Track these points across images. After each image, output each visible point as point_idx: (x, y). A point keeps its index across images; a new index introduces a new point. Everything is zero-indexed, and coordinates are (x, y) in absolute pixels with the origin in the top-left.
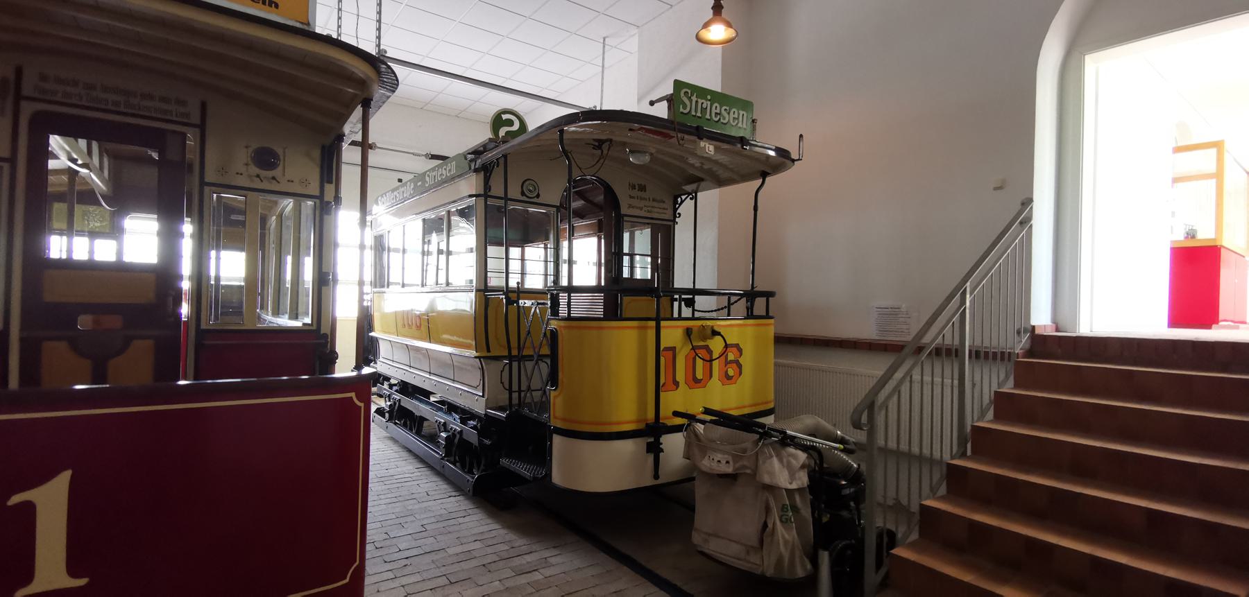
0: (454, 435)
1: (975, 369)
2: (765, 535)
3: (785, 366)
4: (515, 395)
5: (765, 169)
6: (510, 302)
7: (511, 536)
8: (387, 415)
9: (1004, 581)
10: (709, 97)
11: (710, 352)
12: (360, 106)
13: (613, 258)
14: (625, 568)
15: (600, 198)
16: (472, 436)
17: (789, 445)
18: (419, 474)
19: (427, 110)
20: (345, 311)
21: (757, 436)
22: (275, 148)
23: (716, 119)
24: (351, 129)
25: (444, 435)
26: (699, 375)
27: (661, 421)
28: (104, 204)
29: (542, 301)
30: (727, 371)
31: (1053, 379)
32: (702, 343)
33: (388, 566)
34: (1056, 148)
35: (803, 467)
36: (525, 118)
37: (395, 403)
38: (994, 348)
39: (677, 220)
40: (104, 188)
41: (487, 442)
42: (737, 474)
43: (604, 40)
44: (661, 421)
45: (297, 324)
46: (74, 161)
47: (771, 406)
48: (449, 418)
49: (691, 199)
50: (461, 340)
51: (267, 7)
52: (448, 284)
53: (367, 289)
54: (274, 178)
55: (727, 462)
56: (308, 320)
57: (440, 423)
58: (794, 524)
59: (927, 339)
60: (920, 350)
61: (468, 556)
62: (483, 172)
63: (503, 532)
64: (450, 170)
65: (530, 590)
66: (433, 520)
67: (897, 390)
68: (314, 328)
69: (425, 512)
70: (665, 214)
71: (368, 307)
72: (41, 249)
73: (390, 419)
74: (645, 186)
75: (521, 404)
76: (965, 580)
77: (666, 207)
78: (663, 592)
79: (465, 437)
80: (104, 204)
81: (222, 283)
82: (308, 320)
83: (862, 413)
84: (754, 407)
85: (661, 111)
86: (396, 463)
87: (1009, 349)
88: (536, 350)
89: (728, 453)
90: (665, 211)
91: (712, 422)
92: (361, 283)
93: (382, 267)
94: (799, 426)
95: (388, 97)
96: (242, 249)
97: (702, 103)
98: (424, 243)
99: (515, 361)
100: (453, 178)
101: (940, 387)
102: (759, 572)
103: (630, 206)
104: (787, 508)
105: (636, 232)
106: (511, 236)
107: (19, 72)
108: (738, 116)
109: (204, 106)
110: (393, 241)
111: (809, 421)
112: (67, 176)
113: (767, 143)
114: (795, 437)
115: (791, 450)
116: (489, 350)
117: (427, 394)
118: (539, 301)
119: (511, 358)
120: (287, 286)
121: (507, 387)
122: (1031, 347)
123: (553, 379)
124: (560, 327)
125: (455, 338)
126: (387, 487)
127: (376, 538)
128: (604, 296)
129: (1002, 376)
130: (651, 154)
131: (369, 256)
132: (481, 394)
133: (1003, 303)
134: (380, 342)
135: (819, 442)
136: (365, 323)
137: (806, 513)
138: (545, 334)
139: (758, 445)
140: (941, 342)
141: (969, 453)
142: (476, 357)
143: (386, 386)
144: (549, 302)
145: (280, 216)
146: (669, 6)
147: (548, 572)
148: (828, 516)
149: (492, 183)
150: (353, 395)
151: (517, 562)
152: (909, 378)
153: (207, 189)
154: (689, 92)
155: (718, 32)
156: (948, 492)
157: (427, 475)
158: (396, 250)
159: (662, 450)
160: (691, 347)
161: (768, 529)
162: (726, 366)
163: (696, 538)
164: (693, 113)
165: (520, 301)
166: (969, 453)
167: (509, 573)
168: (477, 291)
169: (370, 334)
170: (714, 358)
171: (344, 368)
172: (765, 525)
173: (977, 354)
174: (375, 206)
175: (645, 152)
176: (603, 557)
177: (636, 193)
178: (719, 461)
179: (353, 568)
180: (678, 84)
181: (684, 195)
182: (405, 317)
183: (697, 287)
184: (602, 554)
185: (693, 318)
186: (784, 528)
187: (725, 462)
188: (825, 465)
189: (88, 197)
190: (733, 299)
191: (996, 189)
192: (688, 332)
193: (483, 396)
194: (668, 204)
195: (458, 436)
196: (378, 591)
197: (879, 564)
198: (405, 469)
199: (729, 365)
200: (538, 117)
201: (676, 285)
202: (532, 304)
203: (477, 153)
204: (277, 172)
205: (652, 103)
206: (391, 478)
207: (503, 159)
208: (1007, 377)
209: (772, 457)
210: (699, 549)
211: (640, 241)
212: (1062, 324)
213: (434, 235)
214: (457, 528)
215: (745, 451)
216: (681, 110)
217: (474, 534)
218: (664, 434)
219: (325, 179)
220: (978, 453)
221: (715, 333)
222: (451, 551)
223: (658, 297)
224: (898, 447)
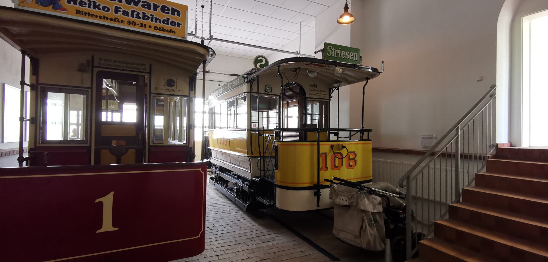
0: (239, 188)
1: (447, 162)
2: (362, 230)
3: (381, 162)
4: (262, 172)
5: (368, 77)
6: (260, 135)
7: (261, 228)
8: (214, 180)
9: (470, 256)
10: (340, 49)
11: (342, 155)
12: (202, 63)
13: (303, 115)
14: (306, 243)
15: (298, 91)
16: (246, 188)
17: (373, 194)
18: (226, 203)
19: (229, 56)
20: (198, 138)
21: (358, 190)
22: (173, 78)
23: (344, 57)
24: (200, 70)
25: (235, 188)
26: (337, 164)
27: (320, 183)
28: (116, 100)
29: (272, 134)
31: (506, 168)
32: (338, 151)
33: (214, 236)
34: (509, 60)
35: (379, 203)
36: (268, 60)
37: (217, 175)
38: (475, 154)
39: (331, 99)
40: (116, 94)
41: (252, 191)
42: (350, 205)
43: (301, 23)
44: (320, 183)
45: (181, 143)
46: (107, 85)
47: (371, 178)
48: (237, 181)
49: (337, 90)
50: (242, 150)
51: (172, 34)
52: (237, 127)
53: (206, 129)
54: (173, 90)
55: (346, 200)
56: (185, 142)
57: (234, 183)
58: (375, 227)
59: (438, 149)
60: (433, 154)
61: (244, 235)
62: (249, 83)
63: (258, 226)
64: (237, 82)
65: (267, 248)
66: (231, 221)
67: (422, 171)
68: (187, 145)
69: (228, 217)
70: (325, 96)
71: (207, 136)
72: (98, 117)
73: (216, 181)
74: (317, 85)
75: (265, 176)
76: (452, 255)
77: (326, 94)
78: (320, 253)
79: (243, 188)
80: (116, 100)
81: (155, 128)
82: (185, 142)
83: (404, 181)
84: (361, 179)
85: (319, 56)
86: (218, 199)
87: (483, 154)
88: (270, 154)
89: (347, 197)
90: (325, 95)
91: (339, 183)
92: (203, 127)
93: (212, 119)
94: (378, 186)
95: (212, 59)
96: (163, 115)
97: (337, 51)
98: (228, 110)
99: (262, 158)
100: (238, 85)
101: (444, 171)
102: (360, 246)
103: (310, 94)
104: (372, 220)
105: (314, 104)
106: (260, 106)
107: (93, 57)
108: (353, 55)
109: (151, 66)
110: (217, 111)
111: (383, 184)
112: (105, 90)
113: (368, 64)
114: (375, 191)
115: (374, 196)
116: (252, 154)
117: (230, 171)
118: (271, 134)
119: (260, 157)
120: (178, 129)
121: (259, 168)
122: (496, 153)
123: (277, 166)
124: (279, 144)
125: (239, 149)
126: (215, 207)
127: (210, 226)
128: (299, 132)
129: (480, 166)
130: (317, 73)
131: (207, 116)
132: (249, 171)
134: (212, 150)
135: (387, 193)
136: (205, 143)
137: (382, 223)
138: (273, 147)
139: (358, 193)
140: (445, 151)
141: (461, 201)
142: (247, 157)
143: (214, 168)
144: (275, 135)
145: (175, 102)
146: (328, 7)
147: (274, 242)
148: (393, 225)
149: (253, 87)
150: (200, 169)
151: (262, 238)
152: (428, 167)
153: (152, 95)
155: (347, 19)
156: (450, 217)
157: (229, 204)
158: (217, 114)
159: (320, 195)
160: (333, 153)
161: (363, 229)
163: (334, 232)
164: (333, 56)
165: (264, 134)
166: (461, 201)
167: (259, 242)
168: (248, 130)
169: (208, 147)
170: (343, 157)
171: (198, 160)
172: (362, 227)
173: (466, 157)
174: (209, 96)
175: (315, 72)
176: (297, 238)
177: (313, 88)
178: (343, 200)
179: (200, 234)
180: (326, 45)
182: (221, 141)
184: (297, 237)
185: (338, 141)
186: (370, 228)
188: (391, 204)
189: (112, 97)
190: (352, 133)
191: (478, 81)
192: (332, 146)
193: (250, 172)
194: (327, 92)
195: (241, 188)
197: (413, 247)
198: (221, 201)
199: (350, 161)
200: (273, 58)
201: (331, 127)
202: (269, 135)
203: (248, 74)
204: (174, 88)
205: (316, 53)
206: (216, 204)
207: (257, 77)
208: (483, 167)
209: (364, 198)
210: (336, 236)
211: (314, 109)
212: (514, 142)
213: (232, 107)
214: (240, 224)
215: (353, 196)
216: (328, 55)
217: (246, 227)
218: (321, 189)
220: (465, 201)
221: (343, 147)
222: (238, 232)
223: (319, 132)
224: (416, 195)
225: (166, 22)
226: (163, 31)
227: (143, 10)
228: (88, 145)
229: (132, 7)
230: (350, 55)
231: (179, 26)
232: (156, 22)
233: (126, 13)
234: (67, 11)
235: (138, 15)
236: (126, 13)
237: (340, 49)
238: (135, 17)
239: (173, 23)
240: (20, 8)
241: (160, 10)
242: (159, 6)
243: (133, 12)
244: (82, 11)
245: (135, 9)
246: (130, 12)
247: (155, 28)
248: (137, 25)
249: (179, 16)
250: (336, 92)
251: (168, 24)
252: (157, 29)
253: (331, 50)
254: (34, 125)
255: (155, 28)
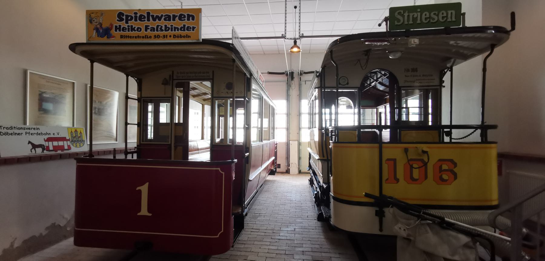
10: (419, 10)
23: (426, 22)
30: (441, 176)
49: (450, 71)
97: (413, 15)
103: (406, 81)
107: (173, 72)
133: (271, 126)
154: (402, 11)
162: (440, 173)
164: (406, 23)
181: (446, 69)
183: (453, 124)
187: (403, 229)
196: (260, 248)
205: (380, 25)
216: (396, 23)
219: (248, 90)
225: (183, 29)
226: (181, 38)
227: (183, 23)
228: (170, 143)
229: (157, 23)
230: (441, 16)
231: (193, 30)
232: (175, 31)
233: (153, 29)
234: (115, 38)
235: (161, 29)
236: (153, 29)
237: (419, 10)
238: (159, 31)
239: (188, 29)
240: (90, 42)
241: (178, 20)
242: (177, 16)
243: (158, 26)
244: (124, 35)
245: (159, 24)
246: (155, 28)
247: (175, 36)
248: (161, 37)
249: (194, 20)
250: (449, 73)
251: (184, 30)
252: (176, 37)
253: (403, 16)
254: (139, 128)
255: (175, 36)
